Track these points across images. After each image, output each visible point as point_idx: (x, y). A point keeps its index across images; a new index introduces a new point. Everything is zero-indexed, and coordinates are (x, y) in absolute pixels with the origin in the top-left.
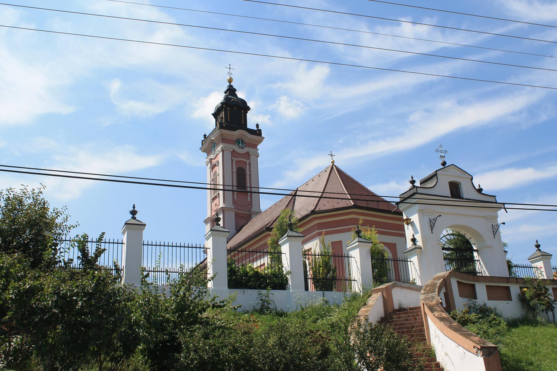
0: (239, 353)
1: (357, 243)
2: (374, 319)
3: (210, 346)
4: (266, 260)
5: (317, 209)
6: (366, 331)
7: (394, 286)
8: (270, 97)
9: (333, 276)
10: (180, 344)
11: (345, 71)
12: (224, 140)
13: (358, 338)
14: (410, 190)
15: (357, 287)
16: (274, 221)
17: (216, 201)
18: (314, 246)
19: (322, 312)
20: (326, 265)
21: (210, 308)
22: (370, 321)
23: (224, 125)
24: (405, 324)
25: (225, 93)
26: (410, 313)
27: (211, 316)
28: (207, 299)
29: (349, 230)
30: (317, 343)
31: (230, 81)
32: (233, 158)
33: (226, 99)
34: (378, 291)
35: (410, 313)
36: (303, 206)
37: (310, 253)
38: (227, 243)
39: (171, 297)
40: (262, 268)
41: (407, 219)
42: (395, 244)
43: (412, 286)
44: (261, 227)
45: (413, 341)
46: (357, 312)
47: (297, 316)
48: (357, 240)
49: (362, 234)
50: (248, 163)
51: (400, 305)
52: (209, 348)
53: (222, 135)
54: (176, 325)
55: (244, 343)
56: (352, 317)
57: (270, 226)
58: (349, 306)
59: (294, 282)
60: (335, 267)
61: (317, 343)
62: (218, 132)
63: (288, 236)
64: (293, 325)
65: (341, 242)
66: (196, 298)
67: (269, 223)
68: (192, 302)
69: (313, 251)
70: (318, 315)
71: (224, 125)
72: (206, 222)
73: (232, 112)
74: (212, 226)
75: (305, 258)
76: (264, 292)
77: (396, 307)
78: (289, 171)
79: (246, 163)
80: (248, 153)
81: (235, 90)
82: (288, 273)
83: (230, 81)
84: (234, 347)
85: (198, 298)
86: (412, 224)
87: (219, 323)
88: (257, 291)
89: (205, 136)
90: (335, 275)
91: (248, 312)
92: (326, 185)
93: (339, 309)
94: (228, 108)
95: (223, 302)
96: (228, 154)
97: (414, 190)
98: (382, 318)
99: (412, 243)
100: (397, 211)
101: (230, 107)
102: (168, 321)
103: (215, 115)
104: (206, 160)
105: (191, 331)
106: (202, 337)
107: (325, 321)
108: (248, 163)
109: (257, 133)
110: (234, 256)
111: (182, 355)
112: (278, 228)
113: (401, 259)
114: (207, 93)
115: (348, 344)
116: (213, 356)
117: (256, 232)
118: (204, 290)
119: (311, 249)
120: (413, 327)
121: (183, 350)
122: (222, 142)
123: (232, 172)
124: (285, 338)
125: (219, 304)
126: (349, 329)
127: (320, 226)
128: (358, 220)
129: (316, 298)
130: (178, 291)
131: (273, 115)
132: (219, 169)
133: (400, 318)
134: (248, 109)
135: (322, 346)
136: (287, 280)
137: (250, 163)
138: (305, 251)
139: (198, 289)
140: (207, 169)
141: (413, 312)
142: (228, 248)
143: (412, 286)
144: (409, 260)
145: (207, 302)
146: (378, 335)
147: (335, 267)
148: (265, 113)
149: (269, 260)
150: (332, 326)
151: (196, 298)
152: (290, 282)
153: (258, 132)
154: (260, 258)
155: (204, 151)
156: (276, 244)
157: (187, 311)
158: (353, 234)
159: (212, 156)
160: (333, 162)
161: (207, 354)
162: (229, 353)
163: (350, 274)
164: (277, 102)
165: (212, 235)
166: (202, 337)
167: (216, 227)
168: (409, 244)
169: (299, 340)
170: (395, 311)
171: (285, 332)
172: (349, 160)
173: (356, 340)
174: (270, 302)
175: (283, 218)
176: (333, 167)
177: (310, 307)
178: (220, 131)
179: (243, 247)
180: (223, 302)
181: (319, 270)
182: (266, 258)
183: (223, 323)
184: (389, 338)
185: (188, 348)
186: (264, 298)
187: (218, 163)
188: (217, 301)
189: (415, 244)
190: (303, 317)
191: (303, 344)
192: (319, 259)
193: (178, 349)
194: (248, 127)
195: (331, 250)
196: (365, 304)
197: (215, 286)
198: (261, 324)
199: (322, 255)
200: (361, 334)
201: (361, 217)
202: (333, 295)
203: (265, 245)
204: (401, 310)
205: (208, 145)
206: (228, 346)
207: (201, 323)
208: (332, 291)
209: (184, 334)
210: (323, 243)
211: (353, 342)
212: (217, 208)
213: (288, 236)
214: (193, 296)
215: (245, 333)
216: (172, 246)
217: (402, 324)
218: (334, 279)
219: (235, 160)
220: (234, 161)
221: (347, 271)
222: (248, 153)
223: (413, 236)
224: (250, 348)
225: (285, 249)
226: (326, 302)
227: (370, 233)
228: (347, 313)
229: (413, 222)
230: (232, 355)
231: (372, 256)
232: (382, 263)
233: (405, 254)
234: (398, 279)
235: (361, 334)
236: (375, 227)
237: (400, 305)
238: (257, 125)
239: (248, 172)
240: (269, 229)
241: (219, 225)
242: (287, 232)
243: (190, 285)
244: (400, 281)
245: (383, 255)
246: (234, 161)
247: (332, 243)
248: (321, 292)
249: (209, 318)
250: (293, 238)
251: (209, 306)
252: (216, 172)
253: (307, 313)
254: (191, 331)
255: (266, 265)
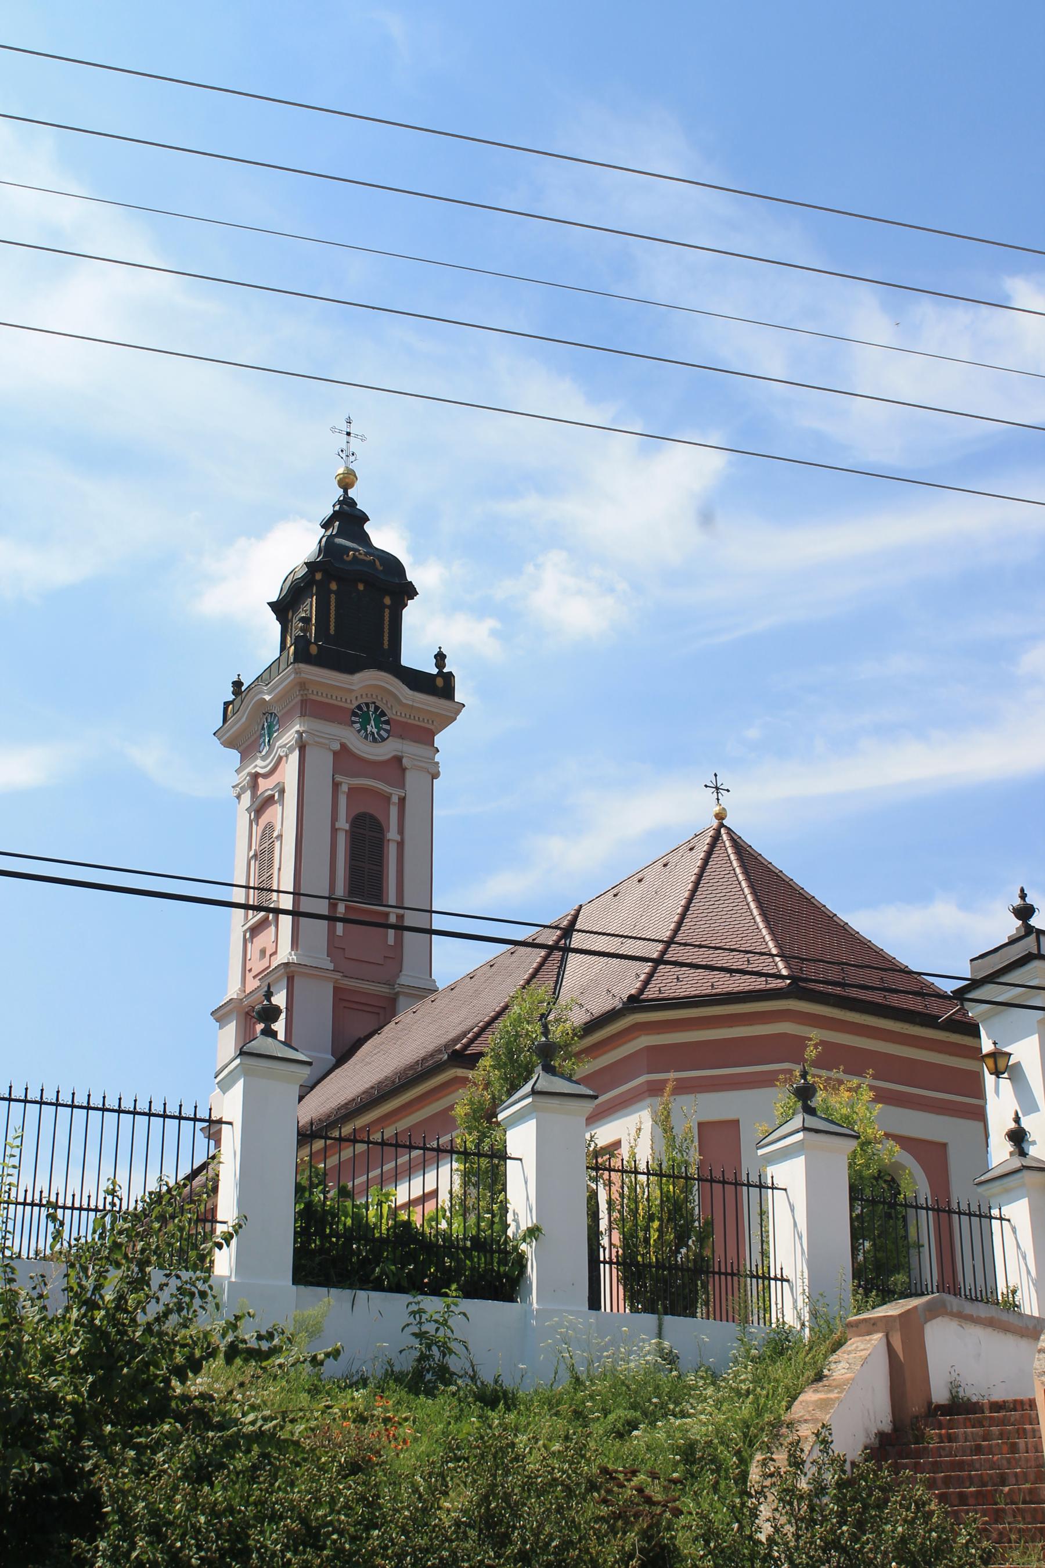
0: (323, 1548)
1: (800, 1136)
2: (850, 1443)
3: (214, 1513)
4: (444, 1179)
5: (651, 993)
6: (820, 1490)
7: (933, 1311)
8: (499, 551)
9: (700, 1258)
10: (94, 1498)
11: (783, 467)
12: (312, 707)
13: (791, 1514)
14: (1013, 941)
15: (790, 1308)
16: (483, 1030)
17: (265, 938)
18: (633, 1134)
19: (652, 1400)
20: (675, 1210)
21: (220, 1361)
22: (838, 1448)
23: (314, 650)
24: (971, 1465)
25: (326, 525)
26: (993, 1422)
27: (219, 1389)
28: (208, 1323)
29: (767, 1081)
30: (627, 1522)
31: (346, 482)
32: (339, 778)
33: (328, 548)
34: (872, 1326)
35: (993, 1422)
36: (590, 986)
37: (616, 1163)
38: (301, 1098)
39: (68, 1309)
40: (430, 1206)
41: (994, 1055)
42: (944, 1146)
43: (1005, 1317)
44: (431, 1048)
45: (1002, 1537)
46: (788, 1408)
47: (552, 1404)
48: (797, 1122)
49: (818, 1100)
50: (395, 799)
51: (954, 1387)
52: (208, 1523)
53: (302, 685)
54: (84, 1422)
55: (347, 1506)
56: (764, 1430)
57: (466, 1046)
58: (757, 1381)
59: (550, 1275)
60: (709, 1224)
61: (627, 1522)
62: (288, 675)
63: (534, 1092)
64: (538, 1444)
65: (734, 1125)
66: (166, 1314)
67: (464, 1034)
68: (148, 1329)
69: (624, 1152)
70: (634, 1407)
71: (314, 650)
72: (220, 1015)
73: (347, 601)
74: (246, 1036)
75: (595, 1180)
76: (432, 1305)
77: (940, 1395)
78: (547, 843)
79: (388, 799)
80: (398, 760)
81: (365, 518)
82: (533, 1232)
83: (346, 482)
84: (304, 1521)
85: (174, 1318)
86: (1015, 1073)
87: (251, 1417)
88: (402, 1299)
89: (237, 684)
90: (707, 1253)
91: (364, 1382)
92: (690, 900)
93: (718, 1389)
94: (334, 586)
95: (270, 1336)
96: (322, 762)
97: (1029, 944)
98: (881, 1435)
99: (1009, 1147)
100: (957, 1017)
101: (339, 580)
102: (52, 1403)
103: (282, 608)
104: (236, 779)
105: (140, 1449)
106: (185, 1477)
107: (661, 1435)
108: (395, 799)
109: (439, 685)
110: (325, 1152)
111: (102, 1545)
112: (497, 1057)
113: (964, 1207)
114: (258, 524)
115: (750, 1537)
116: (222, 1557)
117: (411, 1067)
118: (200, 1285)
119: (617, 1144)
120: (1003, 1480)
121: (108, 1526)
122: (303, 715)
123: (334, 831)
124: (506, 1497)
125: (253, 1344)
126: (755, 1474)
127: (660, 1058)
128: (801, 1042)
129: (630, 1340)
130: (98, 1287)
131: (510, 618)
132: (285, 818)
133: (951, 1438)
134: (410, 592)
135: (645, 1535)
136: (521, 1262)
137: (402, 800)
138: (596, 1154)
139: (174, 1283)
140: (230, 820)
141: (1003, 1422)
142: (304, 1120)
143: (1002, 1315)
144: (995, 1212)
145: (206, 1335)
146: (866, 1507)
147: (709, 1224)
148: (482, 610)
149: (457, 1180)
150: (689, 1453)
151: (166, 1314)
152: (532, 1272)
153: (440, 682)
154: (423, 1167)
155: (229, 744)
156: (486, 1116)
157: (129, 1374)
158: (780, 1097)
159: (260, 765)
160: (720, 816)
161: (200, 1548)
162: (286, 1547)
163: (764, 1254)
164: (530, 569)
165: (244, 1071)
166: (183, 1479)
167: (263, 1044)
168: (1000, 1152)
169: (560, 1510)
170: (934, 1411)
171: (507, 1473)
172: (781, 807)
173: (783, 1520)
174: (453, 1345)
175: (519, 1020)
176: (720, 835)
177: (604, 1377)
178: (297, 672)
179: (360, 1122)
180: (270, 1336)
181: (647, 1229)
182: (445, 1170)
183: (265, 1419)
184: (910, 1523)
185: (125, 1518)
186: (430, 1328)
187: (282, 792)
188: (248, 1335)
189: (1023, 1154)
190: (579, 1415)
191: (574, 1526)
192: (649, 1190)
193: (87, 1518)
194: (406, 661)
195: (694, 1156)
196: (819, 1377)
197: (243, 1268)
198: (414, 1439)
199: (660, 1175)
200: (801, 1497)
201: (815, 1034)
202: (695, 1334)
203: (445, 1119)
204: (959, 1407)
205: (247, 720)
206: (281, 1518)
207: (180, 1418)
208: (693, 1315)
209: (111, 1461)
210: (664, 1123)
211: (767, 1529)
212: (265, 963)
213: (534, 1092)
214: (154, 1309)
215: (354, 1468)
216: (88, 1108)
217: (961, 1466)
218: (701, 1268)
219: (347, 783)
220: (345, 788)
221: (756, 1240)
222: (398, 760)
223: (1017, 1120)
224: (368, 1529)
225: (521, 1140)
226: (671, 1359)
227: (850, 1098)
228: (746, 1410)
229: (1018, 1064)
230: (296, 1553)
231: (852, 1188)
232: (889, 1216)
233: (981, 1189)
234: (950, 1285)
235: (801, 1497)
236: (875, 1077)
237: (954, 1387)
238: (440, 658)
239: (392, 834)
240: (460, 1056)
241: (274, 1034)
242: (530, 1073)
243: (143, 1264)
244: (956, 1292)
245: (893, 1184)
246: (345, 788)
247: (700, 1125)
248: (651, 1319)
249: (211, 1398)
250: (555, 1102)
251: (212, 1354)
252: (270, 827)
253: (592, 1397)
254: (140, 1449)
255: (444, 1197)
